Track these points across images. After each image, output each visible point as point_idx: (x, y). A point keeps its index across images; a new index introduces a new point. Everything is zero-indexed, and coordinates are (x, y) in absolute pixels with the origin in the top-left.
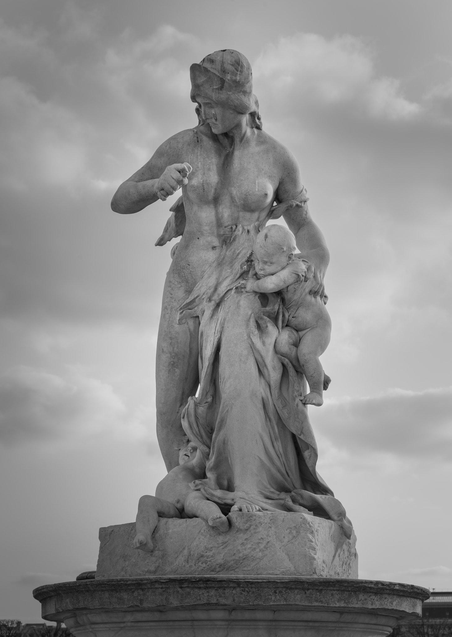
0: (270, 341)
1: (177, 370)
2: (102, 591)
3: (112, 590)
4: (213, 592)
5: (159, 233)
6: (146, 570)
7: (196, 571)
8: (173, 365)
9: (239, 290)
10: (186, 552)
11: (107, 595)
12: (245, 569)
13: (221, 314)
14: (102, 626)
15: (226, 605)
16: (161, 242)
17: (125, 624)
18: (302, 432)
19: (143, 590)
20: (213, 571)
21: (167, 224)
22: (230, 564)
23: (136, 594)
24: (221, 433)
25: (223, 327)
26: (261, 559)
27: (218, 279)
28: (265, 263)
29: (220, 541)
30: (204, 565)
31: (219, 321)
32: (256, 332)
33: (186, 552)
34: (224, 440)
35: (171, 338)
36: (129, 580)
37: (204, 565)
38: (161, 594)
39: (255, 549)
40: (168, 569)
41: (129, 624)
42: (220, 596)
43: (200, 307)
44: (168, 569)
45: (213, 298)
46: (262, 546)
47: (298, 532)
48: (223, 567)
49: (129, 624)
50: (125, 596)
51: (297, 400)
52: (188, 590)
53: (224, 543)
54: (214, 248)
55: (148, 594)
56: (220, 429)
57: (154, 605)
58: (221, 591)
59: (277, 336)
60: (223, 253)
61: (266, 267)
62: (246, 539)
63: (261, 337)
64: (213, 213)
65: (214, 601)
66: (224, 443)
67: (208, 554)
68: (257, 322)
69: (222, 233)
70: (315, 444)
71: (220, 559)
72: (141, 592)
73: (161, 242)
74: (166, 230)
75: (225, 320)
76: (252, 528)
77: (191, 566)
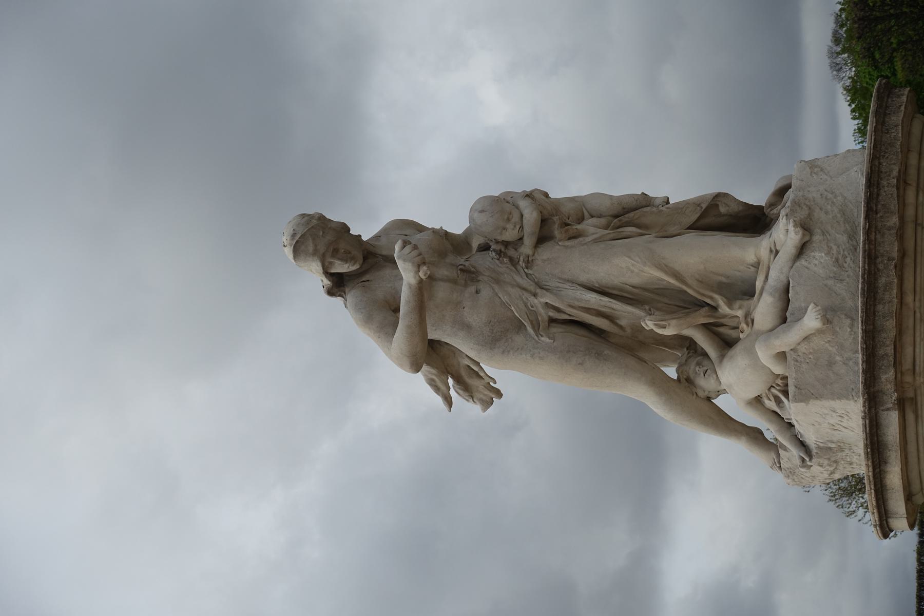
0: (592, 230)
1: (605, 352)
2: (874, 313)
3: (875, 299)
4: (884, 183)
5: (438, 400)
6: (849, 330)
7: (856, 266)
8: (599, 355)
9: (529, 263)
10: (830, 282)
11: (880, 307)
12: (855, 214)
13: (553, 283)
14: (917, 350)
15: (900, 171)
16: (449, 401)
17: (917, 311)
18: (699, 205)
19: (876, 257)
20: (856, 249)
21: (430, 385)
22: (849, 228)
23: (881, 266)
24: (690, 281)
25: (568, 281)
26: (845, 198)
27: (513, 286)
28: (508, 220)
29: (821, 238)
30: (848, 260)
31: (561, 285)
32: (581, 239)
33: (830, 282)
34: (698, 280)
35: (568, 352)
36: (864, 266)
37: (848, 260)
38: (883, 236)
39: (833, 202)
40: (850, 303)
41: (917, 304)
42: (889, 175)
43: (542, 311)
44: (850, 303)
45: (533, 290)
46: (830, 196)
47: (816, 167)
48: (852, 236)
49: (917, 304)
50: (882, 280)
51: (663, 208)
52: (879, 206)
53: (823, 234)
54: (477, 292)
55: (882, 251)
56: (683, 281)
57: (896, 243)
58: (882, 175)
59: (590, 226)
60: (486, 279)
61: (513, 220)
62: (821, 209)
63: (587, 236)
64: (442, 284)
65: (895, 181)
66: (701, 282)
67: (835, 252)
68: (570, 239)
69: (463, 282)
70: (711, 194)
71: (843, 239)
72: (879, 259)
73: (449, 401)
74: (437, 389)
75: (560, 278)
76: (807, 202)
77: (848, 276)
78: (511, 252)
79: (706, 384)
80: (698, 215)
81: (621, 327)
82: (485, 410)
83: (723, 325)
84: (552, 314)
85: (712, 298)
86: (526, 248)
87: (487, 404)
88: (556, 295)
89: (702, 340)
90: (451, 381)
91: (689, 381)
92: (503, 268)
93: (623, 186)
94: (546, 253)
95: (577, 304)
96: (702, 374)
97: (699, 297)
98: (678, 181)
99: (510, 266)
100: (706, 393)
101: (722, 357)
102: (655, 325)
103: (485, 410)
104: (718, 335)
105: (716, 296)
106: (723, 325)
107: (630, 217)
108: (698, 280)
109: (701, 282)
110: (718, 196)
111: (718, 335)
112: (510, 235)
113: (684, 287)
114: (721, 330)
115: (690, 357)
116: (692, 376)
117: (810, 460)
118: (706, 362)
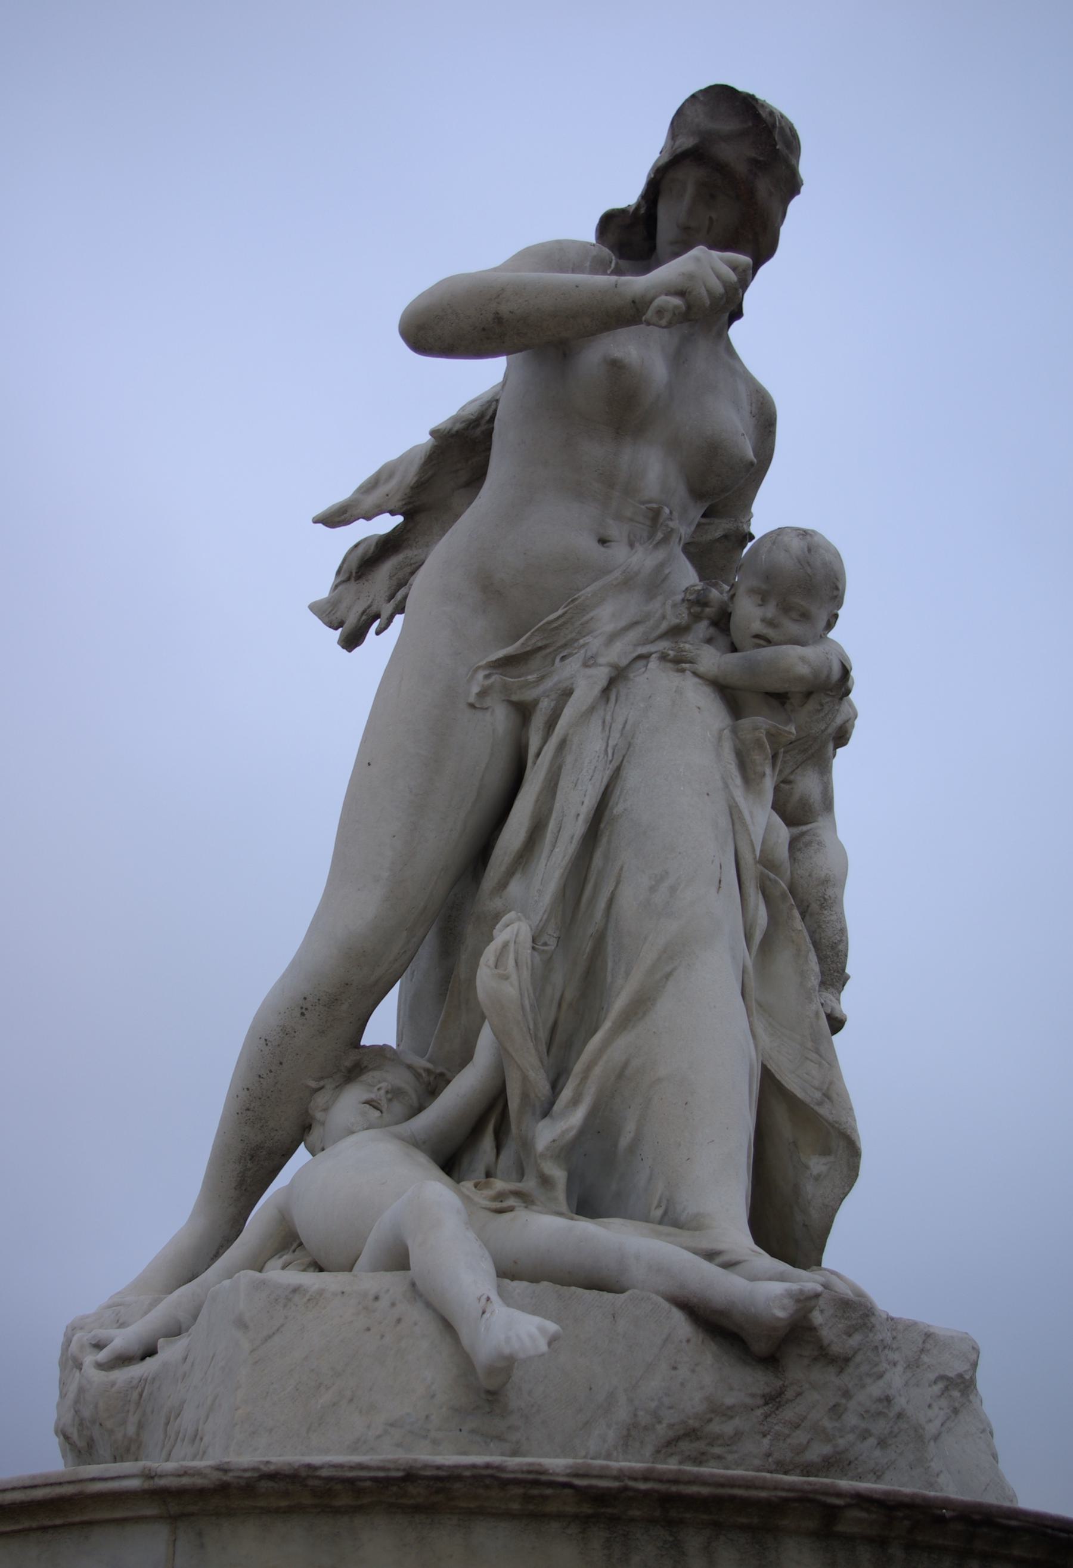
5: (342, 492)
9: (679, 662)
18: (827, 1096)
24: (623, 1042)
32: (738, 781)
34: (626, 1065)
67: (715, 1427)
70: (855, 1130)
78: (702, 628)
79: (348, 1105)
80: (799, 1094)
81: (503, 885)
82: (316, 609)
83: (499, 1147)
84: (545, 706)
85: (575, 1102)
86: (712, 659)
87: (328, 613)
88: (592, 709)
89: (464, 1087)
90: (386, 524)
91: (353, 1073)
92: (669, 610)
93: (867, 915)
94: (706, 713)
95: (569, 759)
96: (366, 1096)
97: (578, 1067)
98: (881, 1057)
99: (664, 626)
100: (319, 1115)
101: (415, 1143)
102: (506, 945)
103: (316, 609)
104: (475, 1132)
105: (577, 1117)
106: (499, 1147)
107: (797, 920)
108: (626, 1065)
109: (620, 1075)
110: (853, 1152)
111: (475, 1132)
112: (749, 613)
113: (607, 1025)
114: (487, 1142)
115: (417, 1076)
116: (367, 1077)
117: (100, 1366)
118: (398, 1108)
